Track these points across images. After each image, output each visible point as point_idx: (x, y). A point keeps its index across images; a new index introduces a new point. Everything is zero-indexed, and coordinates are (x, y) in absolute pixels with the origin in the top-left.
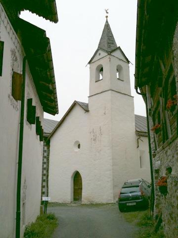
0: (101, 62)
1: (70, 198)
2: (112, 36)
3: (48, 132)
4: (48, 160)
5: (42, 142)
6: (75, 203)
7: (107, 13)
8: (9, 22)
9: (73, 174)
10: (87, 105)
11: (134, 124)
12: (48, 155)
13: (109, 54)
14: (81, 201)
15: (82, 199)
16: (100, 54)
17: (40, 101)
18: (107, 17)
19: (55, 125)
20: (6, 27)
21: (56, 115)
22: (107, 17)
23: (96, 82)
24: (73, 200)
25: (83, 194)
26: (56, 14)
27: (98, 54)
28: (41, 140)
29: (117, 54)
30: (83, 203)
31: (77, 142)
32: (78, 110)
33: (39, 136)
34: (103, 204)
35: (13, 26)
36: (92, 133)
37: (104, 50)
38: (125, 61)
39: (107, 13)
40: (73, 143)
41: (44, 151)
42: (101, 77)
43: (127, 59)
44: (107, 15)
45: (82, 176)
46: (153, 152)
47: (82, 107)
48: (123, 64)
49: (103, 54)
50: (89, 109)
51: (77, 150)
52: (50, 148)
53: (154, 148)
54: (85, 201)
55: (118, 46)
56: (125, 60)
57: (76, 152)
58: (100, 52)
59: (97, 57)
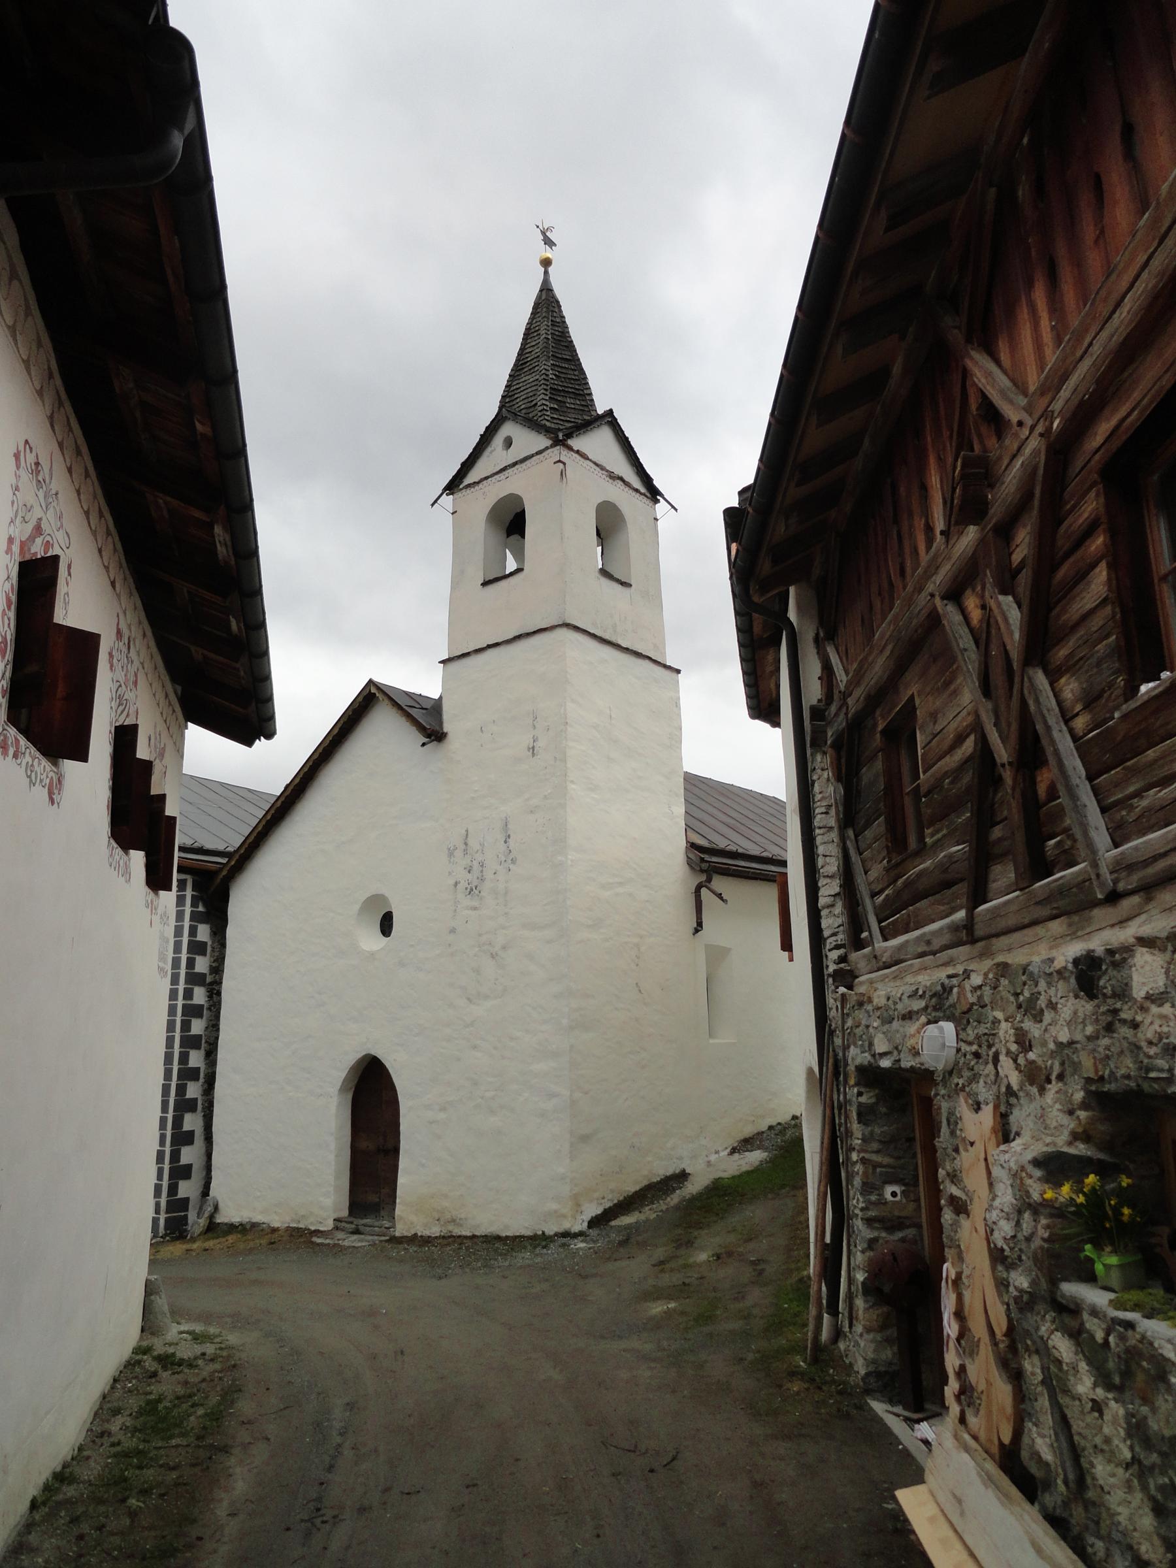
0: (514, 484)
1: (328, 1202)
2: (570, 346)
3: (221, 847)
4: (214, 993)
5: (168, 898)
6: (357, 1232)
7: (549, 242)
8: (85, 450)
9: (353, 1069)
10: (435, 708)
11: (680, 809)
12: (217, 968)
13: (557, 442)
14: (392, 1217)
15: (399, 1210)
16: (508, 443)
17: (28, 270)
18: (546, 263)
19: (256, 814)
20: (151, 684)
21: (261, 744)
22: (546, 263)
23: (485, 584)
24: (345, 1213)
25: (402, 1180)
26: (257, 592)
27: (498, 440)
28: (157, 880)
29: (597, 443)
30: (400, 1230)
31: (376, 900)
32: (382, 722)
33: (138, 858)
34: (516, 1242)
35: (96, 468)
36: (459, 853)
37: (533, 424)
38: (643, 490)
39: (549, 242)
40: (357, 907)
41: (197, 948)
42: (511, 565)
43: (646, 480)
44: (549, 254)
45: (391, 1071)
46: (834, 955)
47: (409, 717)
48: (630, 503)
49: (526, 440)
50: (447, 727)
51: (372, 941)
52: (230, 932)
53: (841, 938)
54: (413, 1218)
55: (600, 411)
56: (636, 483)
57: (372, 955)
58: (509, 429)
59: (496, 456)
